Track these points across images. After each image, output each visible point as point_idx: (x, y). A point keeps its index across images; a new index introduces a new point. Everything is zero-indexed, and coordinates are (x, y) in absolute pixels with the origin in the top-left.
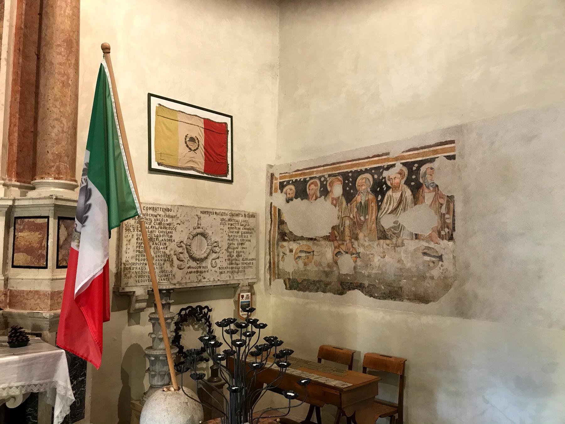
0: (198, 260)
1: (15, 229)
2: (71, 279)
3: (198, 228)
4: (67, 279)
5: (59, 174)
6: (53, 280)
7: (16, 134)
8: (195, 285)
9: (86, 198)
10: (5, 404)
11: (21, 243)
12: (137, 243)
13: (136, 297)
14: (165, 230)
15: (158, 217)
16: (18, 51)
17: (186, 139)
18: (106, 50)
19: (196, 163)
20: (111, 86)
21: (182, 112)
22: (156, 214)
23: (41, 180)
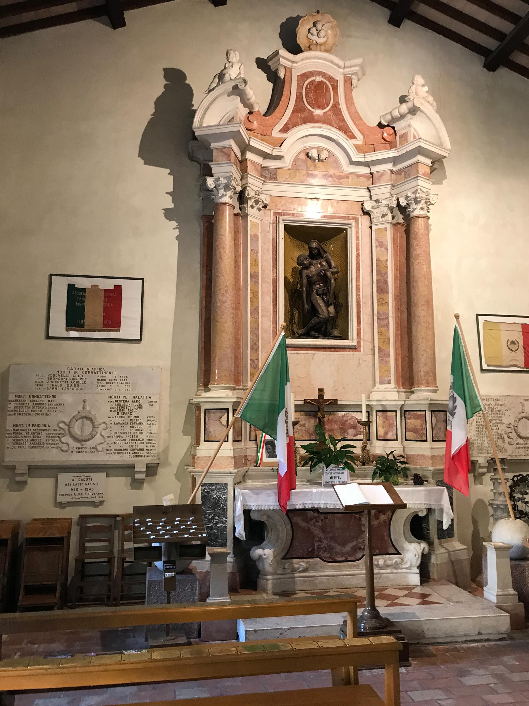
0: (524, 438)
1: (405, 417)
2: (449, 447)
3: (523, 413)
4: (446, 448)
5: (428, 384)
6: (432, 448)
7: (400, 360)
8: (523, 458)
9: (453, 401)
10: (417, 515)
11: (409, 426)
12: (477, 425)
13: (479, 464)
14: (496, 415)
15: (491, 406)
16: (397, 310)
17: (507, 343)
18: (457, 317)
19: (518, 360)
20: (461, 337)
21: (503, 323)
22: (489, 403)
23: (419, 388)
